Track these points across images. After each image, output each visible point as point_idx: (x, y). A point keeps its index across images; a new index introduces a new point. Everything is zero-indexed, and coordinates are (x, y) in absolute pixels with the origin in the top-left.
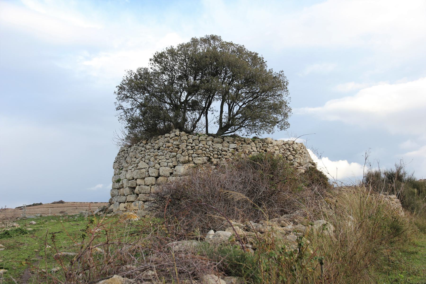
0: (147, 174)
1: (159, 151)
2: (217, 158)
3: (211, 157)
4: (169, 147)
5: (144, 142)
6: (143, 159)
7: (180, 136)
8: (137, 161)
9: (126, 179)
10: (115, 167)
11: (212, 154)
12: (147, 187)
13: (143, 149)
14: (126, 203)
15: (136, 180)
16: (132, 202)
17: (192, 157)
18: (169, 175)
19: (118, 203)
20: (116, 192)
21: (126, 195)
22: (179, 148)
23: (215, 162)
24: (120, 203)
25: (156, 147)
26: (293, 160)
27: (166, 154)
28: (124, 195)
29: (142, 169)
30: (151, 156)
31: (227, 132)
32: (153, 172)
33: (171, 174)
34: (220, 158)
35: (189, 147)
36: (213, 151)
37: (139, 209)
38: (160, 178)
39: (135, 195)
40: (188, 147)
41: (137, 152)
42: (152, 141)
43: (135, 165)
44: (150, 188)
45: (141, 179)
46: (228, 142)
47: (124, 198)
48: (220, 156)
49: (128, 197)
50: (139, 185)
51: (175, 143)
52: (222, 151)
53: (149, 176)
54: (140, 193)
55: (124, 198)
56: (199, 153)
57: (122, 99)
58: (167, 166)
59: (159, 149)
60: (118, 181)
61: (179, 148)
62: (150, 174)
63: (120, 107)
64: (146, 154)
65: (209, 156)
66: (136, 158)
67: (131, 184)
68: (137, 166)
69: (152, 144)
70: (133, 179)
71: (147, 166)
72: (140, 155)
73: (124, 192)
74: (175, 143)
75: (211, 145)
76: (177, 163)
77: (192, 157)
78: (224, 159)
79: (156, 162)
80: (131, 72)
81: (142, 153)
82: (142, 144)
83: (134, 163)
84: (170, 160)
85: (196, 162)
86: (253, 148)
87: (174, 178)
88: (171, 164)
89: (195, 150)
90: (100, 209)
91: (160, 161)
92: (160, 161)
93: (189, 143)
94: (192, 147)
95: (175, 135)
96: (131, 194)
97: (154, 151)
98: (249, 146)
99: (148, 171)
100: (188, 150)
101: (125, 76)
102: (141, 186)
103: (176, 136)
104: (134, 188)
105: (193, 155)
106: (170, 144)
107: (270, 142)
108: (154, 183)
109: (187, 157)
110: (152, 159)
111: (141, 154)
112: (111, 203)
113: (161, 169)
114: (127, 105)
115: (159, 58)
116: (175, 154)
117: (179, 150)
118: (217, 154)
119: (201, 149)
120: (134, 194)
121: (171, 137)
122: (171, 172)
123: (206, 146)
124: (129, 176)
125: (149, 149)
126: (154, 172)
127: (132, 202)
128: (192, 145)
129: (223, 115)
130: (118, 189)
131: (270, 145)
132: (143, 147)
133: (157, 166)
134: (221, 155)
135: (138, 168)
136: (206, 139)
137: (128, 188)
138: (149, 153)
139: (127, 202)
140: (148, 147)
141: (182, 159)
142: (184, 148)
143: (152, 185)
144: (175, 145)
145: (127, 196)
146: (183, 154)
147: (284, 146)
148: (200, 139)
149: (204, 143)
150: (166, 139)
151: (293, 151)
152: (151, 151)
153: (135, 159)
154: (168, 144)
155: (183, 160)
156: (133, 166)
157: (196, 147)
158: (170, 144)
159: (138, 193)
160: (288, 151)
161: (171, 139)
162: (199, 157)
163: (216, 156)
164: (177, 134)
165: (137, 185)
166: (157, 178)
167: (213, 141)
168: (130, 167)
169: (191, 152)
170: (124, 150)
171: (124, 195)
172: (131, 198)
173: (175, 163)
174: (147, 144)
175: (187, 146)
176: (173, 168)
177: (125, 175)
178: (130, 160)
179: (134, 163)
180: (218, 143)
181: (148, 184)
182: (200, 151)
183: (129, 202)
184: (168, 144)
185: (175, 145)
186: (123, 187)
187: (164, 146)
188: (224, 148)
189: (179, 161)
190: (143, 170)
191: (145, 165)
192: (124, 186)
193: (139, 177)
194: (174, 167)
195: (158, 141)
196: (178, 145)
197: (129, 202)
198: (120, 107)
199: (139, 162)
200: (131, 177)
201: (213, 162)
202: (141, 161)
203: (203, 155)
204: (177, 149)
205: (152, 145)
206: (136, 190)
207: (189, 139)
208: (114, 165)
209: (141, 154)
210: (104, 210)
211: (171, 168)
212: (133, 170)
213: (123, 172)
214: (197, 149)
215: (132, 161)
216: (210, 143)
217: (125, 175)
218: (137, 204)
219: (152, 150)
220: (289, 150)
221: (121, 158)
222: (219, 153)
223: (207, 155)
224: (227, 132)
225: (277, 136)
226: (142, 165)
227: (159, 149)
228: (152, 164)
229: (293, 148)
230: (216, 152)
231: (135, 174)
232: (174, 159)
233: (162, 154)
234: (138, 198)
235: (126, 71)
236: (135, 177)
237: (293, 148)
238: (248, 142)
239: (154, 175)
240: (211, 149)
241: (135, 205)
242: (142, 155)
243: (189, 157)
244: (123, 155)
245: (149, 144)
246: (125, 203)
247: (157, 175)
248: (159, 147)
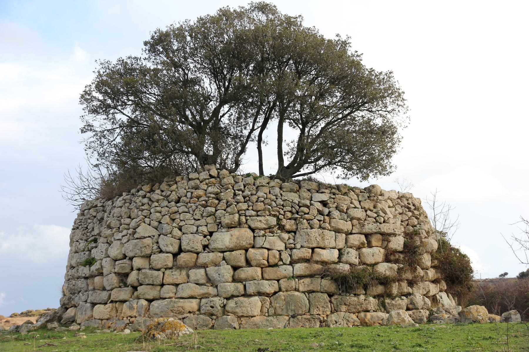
0: (155, 247)
1: (178, 205)
2: (290, 219)
3: (281, 217)
4: (198, 197)
5: (147, 188)
6: (147, 220)
7: (218, 177)
8: (133, 224)
9: (108, 259)
10: (76, 238)
11: (282, 212)
12: (156, 273)
13: (146, 200)
14: (109, 305)
15: (131, 259)
16: (123, 302)
17: (246, 216)
18: (200, 249)
19: (88, 305)
20: (81, 284)
21: (108, 288)
22: (219, 200)
23: (288, 227)
24: (94, 304)
25: (174, 196)
26: (418, 226)
27: (194, 211)
28: (104, 289)
29: (145, 238)
30: (163, 213)
31: (298, 173)
32: (169, 244)
33: (205, 247)
34: (295, 219)
35: (240, 198)
36: (283, 205)
37: (140, 315)
38: (182, 255)
39: (130, 288)
40: (238, 197)
41: (132, 206)
42: (164, 186)
43: (131, 231)
44: (162, 275)
45: (143, 257)
46: (309, 190)
47: (104, 295)
48: (296, 216)
49: (113, 292)
50: (139, 269)
51: (210, 189)
52: (300, 207)
53: (161, 251)
54: (141, 285)
55: (104, 295)
56: (259, 208)
57: (94, 111)
58: (197, 232)
59: (178, 201)
60: (90, 262)
61: (219, 200)
62: (163, 249)
63: (89, 127)
64: (152, 211)
65: (278, 214)
66: (130, 217)
67: (121, 267)
68: (134, 233)
69: (162, 191)
70: (125, 257)
71: (155, 233)
72: (140, 213)
73: (106, 284)
74: (210, 189)
75: (279, 195)
76: (216, 227)
77: (246, 216)
78: (305, 221)
79: (174, 225)
80: (105, 64)
81: (143, 207)
82: (141, 193)
83: (126, 226)
84: (203, 222)
85: (253, 226)
86: (353, 201)
87: (211, 254)
88: (204, 229)
89: (250, 204)
90: (48, 318)
91: (181, 224)
92: (181, 224)
93: (238, 190)
94: (244, 197)
95: (210, 175)
96: (120, 287)
97: (169, 205)
98: (346, 197)
99: (157, 243)
100: (238, 203)
101: (96, 71)
102: (143, 271)
103: (211, 176)
104: (126, 275)
105: (248, 213)
106: (200, 192)
107: (379, 193)
108: (170, 265)
109: (237, 215)
110: (167, 219)
111: (142, 210)
112: (65, 307)
113: (184, 237)
114: (100, 122)
115: (159, 42)
116: (213, 210)
117: (221, 203)
118: (290, 212)
119: (263, 202)
120: (126, 285)
121: (201, 178)
122: (206, 243)
123: (269, 196)
124: (115, 251)
125: (158, 201)
126: (172, 245)
127: (123, 302)
128: (245, 194)
129: (284, 145)
130: (86, 278)
131: (380, 197)
132: (144, 197)
133: (177, 232)
134: (297, 213)
135: (136, 236)
136: (268, 183)
137: (114, 275)
138: (159, 209)
139: (112, 302)
140: (156, 196)
141: (226, 220)
142: (230, 199)
143: (166, 269)
144: (210, 193)
145: (112, 290)
146: (229, 209)
147: (399, 201)
148: (258, 183)
149: (267, 191)
150: (192, 183)
151: (415, 209)
152: (162, 205)
153: (128, 221)
154: (197, 193)
155: (229, 222)
156: (125, 232)
157: (254, 198)
158: (200, 192)
159: (136, 284)
160: (407, 210)
161: (201, 182)
162: (258, 216)
163: (289, 215)
164: (213, 174)
165: (132, 269)
166: (175, 255)
167: (281, 188)
168: (119, 236)
169: (244, 206)
170: (96, 206)
171: (104, 289)
172: (124, 294)
173: (212, 227)
174: (152, 191)
175: (235, 194)
176: (208, 237)
177: (107, 250)
178: (118, 222)
179: (126, 226)
180: (291, 191)
181: (159, 266)
182: (260, 206)
183: (116, 302)
184: (197, 193)
185: (210, 193)
186: (101, 274)
187: (189, 195)
188: (303, 201)
189: (220, 223)
190: (148, 241)
191: (153, 232)
192: (105, 271)
193: (139, 253)
194: (211, 234)
195: (175, 186)
196: (217, 194)
197: (116, 302)
198: (88, 128)
199: (139, 226)
200: (119, 253)
201: (284, 226)
202: (143, 224)
203: (267, 212)
204: (217, 202)
205: (164, 194)
206: (133, 278)
207: (236, 182)
208: (73, 233)
209: (142, 210)
210: (56, 317)
211: (205, 236)
212: (125, 240)
213: (102, 245)
214: (255, 200)
215: (121, 224)
216: (277, 190)
217: (107, 250)
218: (135, 305)
219: (165, 203)
220: (409, 208)
221: (89, 221)
222: (294, 211)
223: (273, 213)
224: (298, 173)
225: (382, 182)
226: (144, 230)
227: (178, 201)
228: (166, 228)
229: (414, 205)
230: (290, 209)
231: (129, 249)
232: (210, 220)
233: (186, 210)
234: (136, 293)
235: (98, 61)
236: (130, 254)
237: (414, 205)
238: (344, 191)
239: (171, 249)
240: (280, 201)
241: (131, 308)
242: (145, 213)
243: (240, 215)
244: (94, 214)
245: (158, 191)
246: (106, 304)
247: (176, 249)
248: (179, 198)
